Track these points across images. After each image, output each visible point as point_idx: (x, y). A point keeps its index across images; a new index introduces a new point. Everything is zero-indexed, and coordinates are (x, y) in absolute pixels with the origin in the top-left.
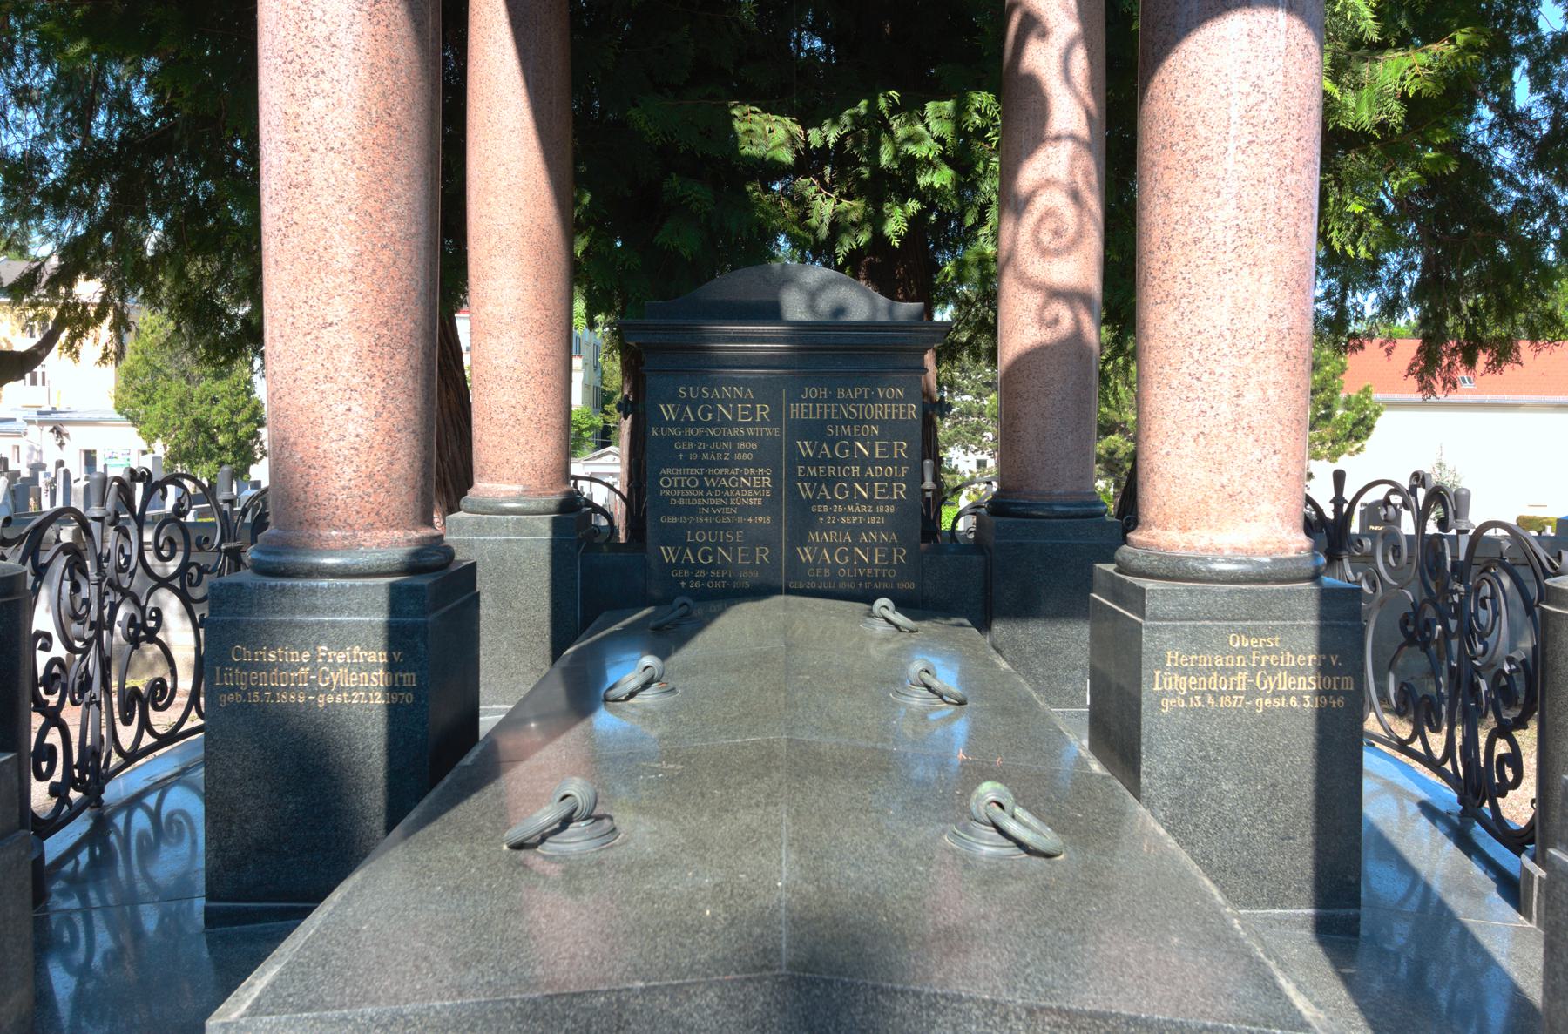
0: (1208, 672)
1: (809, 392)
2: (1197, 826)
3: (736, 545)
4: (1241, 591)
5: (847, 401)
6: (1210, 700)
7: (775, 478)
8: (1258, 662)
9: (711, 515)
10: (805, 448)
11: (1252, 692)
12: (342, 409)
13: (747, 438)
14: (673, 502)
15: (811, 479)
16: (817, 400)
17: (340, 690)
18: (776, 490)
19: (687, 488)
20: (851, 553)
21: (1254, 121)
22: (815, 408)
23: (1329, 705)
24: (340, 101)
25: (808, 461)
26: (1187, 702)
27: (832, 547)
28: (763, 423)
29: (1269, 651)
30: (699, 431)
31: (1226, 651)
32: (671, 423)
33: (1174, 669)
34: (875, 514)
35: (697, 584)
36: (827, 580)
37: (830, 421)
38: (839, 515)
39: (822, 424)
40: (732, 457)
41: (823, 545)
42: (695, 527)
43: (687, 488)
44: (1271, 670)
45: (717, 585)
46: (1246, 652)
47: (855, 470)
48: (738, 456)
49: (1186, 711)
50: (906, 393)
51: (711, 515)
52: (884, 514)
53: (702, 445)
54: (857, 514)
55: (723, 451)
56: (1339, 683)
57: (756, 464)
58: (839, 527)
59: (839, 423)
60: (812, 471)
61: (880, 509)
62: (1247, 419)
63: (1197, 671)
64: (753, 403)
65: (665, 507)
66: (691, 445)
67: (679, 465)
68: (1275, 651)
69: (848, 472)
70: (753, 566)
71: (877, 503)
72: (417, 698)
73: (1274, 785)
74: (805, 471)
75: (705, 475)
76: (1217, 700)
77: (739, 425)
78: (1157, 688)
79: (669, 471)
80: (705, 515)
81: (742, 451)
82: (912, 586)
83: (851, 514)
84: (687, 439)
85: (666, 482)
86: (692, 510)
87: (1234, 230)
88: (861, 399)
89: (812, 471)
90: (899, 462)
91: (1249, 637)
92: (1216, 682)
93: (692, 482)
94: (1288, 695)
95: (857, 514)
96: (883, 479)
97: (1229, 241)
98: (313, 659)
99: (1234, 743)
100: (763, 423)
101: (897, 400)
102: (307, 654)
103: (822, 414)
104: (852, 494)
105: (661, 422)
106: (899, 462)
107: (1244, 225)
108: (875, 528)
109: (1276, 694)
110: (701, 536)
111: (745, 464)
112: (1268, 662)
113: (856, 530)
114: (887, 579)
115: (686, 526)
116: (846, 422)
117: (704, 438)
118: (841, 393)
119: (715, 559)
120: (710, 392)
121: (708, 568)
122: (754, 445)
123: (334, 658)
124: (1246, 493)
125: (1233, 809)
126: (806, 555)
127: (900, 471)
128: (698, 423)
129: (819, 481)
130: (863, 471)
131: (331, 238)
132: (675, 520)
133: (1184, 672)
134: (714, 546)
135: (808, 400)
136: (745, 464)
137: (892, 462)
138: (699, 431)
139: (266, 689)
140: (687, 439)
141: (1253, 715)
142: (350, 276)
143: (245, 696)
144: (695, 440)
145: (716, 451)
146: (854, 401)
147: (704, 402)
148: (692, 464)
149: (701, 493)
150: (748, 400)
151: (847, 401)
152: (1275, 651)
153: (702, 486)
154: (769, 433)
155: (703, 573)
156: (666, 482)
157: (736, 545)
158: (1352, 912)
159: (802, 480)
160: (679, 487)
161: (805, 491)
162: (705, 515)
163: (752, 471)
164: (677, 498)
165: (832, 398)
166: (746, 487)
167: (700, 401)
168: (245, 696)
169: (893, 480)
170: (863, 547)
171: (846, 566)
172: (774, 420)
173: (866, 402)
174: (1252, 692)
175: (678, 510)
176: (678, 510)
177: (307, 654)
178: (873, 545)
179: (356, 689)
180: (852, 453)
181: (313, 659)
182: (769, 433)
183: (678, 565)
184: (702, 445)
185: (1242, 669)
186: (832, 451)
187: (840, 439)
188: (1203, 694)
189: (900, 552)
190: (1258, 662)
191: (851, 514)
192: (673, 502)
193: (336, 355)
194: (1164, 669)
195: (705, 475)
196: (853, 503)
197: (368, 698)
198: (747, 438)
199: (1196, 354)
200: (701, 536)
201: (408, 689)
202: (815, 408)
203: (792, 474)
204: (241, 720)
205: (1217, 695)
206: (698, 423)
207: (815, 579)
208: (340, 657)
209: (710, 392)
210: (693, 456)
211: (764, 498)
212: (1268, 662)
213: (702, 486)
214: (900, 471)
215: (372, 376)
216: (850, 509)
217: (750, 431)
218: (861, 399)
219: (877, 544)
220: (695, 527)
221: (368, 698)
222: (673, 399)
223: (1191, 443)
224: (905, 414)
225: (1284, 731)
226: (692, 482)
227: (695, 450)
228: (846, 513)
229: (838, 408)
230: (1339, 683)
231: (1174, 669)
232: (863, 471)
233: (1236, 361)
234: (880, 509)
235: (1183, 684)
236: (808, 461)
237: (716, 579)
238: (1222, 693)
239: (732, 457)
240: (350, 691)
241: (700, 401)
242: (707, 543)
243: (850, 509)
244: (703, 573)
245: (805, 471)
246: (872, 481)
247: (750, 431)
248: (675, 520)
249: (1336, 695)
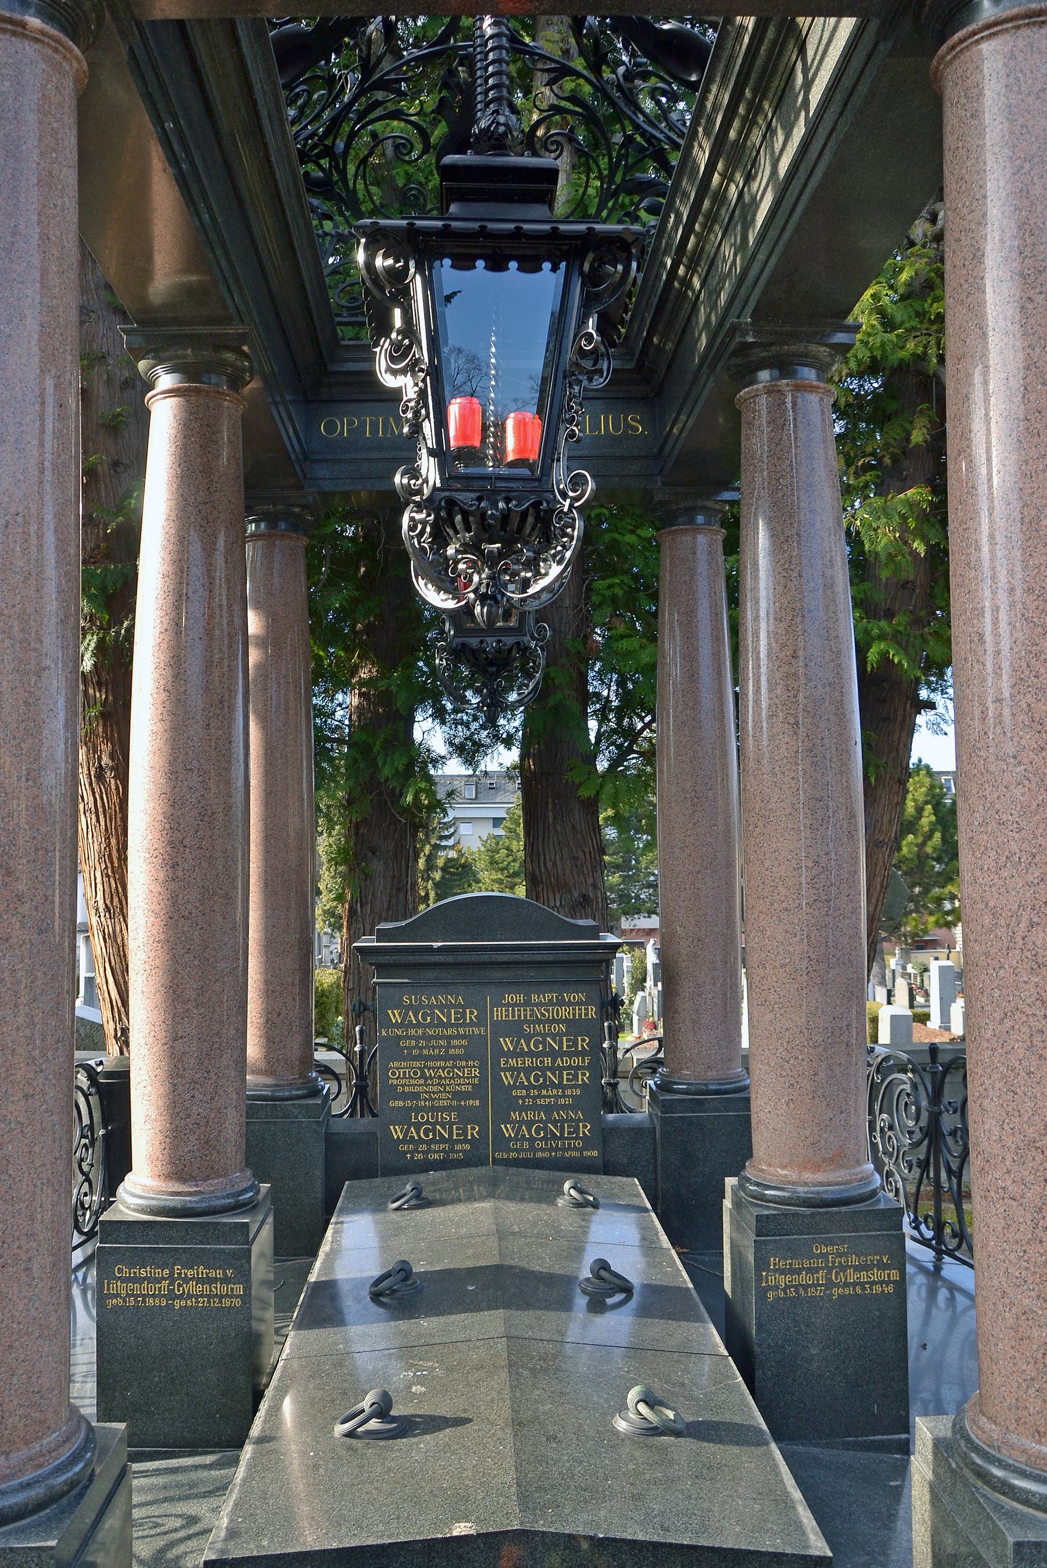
0: (798, 1271)
1: (508, 998)
2: (794, 1380)
3: (451, 1124)
4: (820, 1213)
5: (539, 1005)
6: (801, 1291)
7: (483, 1068)
8: (834, 1262)
9: (431, 1099)
10: (506, 1044)
11: (830, 1285)
12: (188, 1096)
13: (459, 1037)
14: (400, 1089)
15: (512, 1069)
16: (515, 1005)
17: (190, 1296)
18: (483, 1078)
19: (411, 1077)
20: (545, 1129)
21: (817, 886)
22: (513, 1010)
23: (883, 1291)
24: (189, 884)
25: (509, 1054)
26: (785, 1293)
27: (529, 1124)
28: (472, 1024)
29: (840, 1255)
30: (420, 1032)
31: (811, 1256)
32: (397, 1025)
33: (775, 1271)
34: (564, 1096)
35: (420, 1156)
36: (526, 1150)
37: (526, 1021)
38: (534, 1098)
39: (520, 1023)
40: (447, 1051)
41: (522, 1122)
42: (418, 1110)
43: (411, 1077)
44: (843, 1268)
45: (436, 1156)
46: (824, 1256)
47: (547, 1061)
48: (452, 1052)
49: (784, 1299)
50: (586, 997)
51: (431, 1099)
52: (572, 1096)
53: (422, 1043)
54: (549, 1097)
55: (440, 1047)
56: (889, 1275)
57: (466, 1058)
58: (535, 1108)
59: (534, 1023)
60: (512, 1062)
61: (568, 1092)
62: (822, 1090)
63: (792, 1271)
64: (464, 1008)
65: (392, 1092)
66: (413, 1042)
67: (404, 1059)
68: (844, 1254)
69: (542, 1062)
70: (466, 1141)
71: (565, 1088)
72: (244, 1302)
73: (847, 1349)
74: (507, 1062)
75: (426, 1067)
76: (806, 1292)
77: (452, 1026)
78: (764, 1284)
79: (396, 1064)
80: (426, 1100)
81: (455, 1047)
82: (595, 1153)
83: (544, 1097)
84: (411, 1038)
85: (394, 1073)
86: (415, 1096)
87: (807, 960)
88: (551, 1003)
89: (512, 1062)
90: (583, 1053)
91: (826, 1246)
92: (804, 1278)
93: (415, 1073)
94: (854, 1285)
95: (549, 1097)
96: (570, 1067)
97: (804, 967)
98: (172, 1274)
99: (818, 1321)
100: (472, 1024)
101: (580, 1003)
102: (166, 1271)
103: (520, 1016)
104: (545, 1080)
105: (389, 1024)
106: (583, 1053)
107: (813, 956)
108: (564, 1107)
109: (846, 1285)
110: (423, 1117)
111: (459, 1057)
112: (840, 1262)
113: (548, 1109)
114: (575, 1149)
115: (410, 1109)
116: (539, 1022)
117: (424, 1037)
118: (534, 998)
119: (434, 1135)
120: (429, 999)
121: (429, 1143)
122: (464, 1042)
123: (186, 1274)
124: (823, 1142)
125: (819, 1368)
126: (508, 1130)
127: (583, 1061)
128: (419, 1025)
129: (518, 1070)
130: (554, 1061)
131: (182, 978)
132: (401, 1104)
133: (783, 1272)
134: (434, 1125)
135: (508, 1005)
136: (459, 1057)
137: (577, 1054)
138: (420, 1032)
139: (138, 1296)
140: (411, 1038)
141: (831, 1300)
142: (194, 1004)
143: (125, 1301)
144: (417, 1038)
145: (434, 1047)
146: (545, 1004)
147: (424, 1007)
148: (415, 1058)
149: (422, 1081)
150: (460, 1006)
151: (539, 1005)
152: (844, 1254)
153: (423, 1076)
154: (476, 1032)
155: (424, 1147)
156: (394, 1073)
157: (451, 1124)
158: (904, 1436)
159: (505, 1070)
160: (405, 1077)
161: (507, 1079)
162: (426, 1100)
163: (464, 1063)
164: (403, 1086)
165: (527, 1003)
166: (459, 1077)
167: (420, 1007)
168: (125, 1301)
169: (578, 1068)
170: (555, 1123)
171: (541, 1139)
172: (481, 1022)
173: (554, 1005)
174: (830, 1285)
175: (404, 1096)
176: (404, 1096)
177: (166, 1271)
178: (563, 1121)
179: (201, 1296)
180: (544, 1047)
181: (172, 1274)
182: (476, 1032)
183: (404, 1141)
184: (422, 1043)
185: (822, 1268)
186: (528, 1045)
187: (534, 1035)
188: (796, 1287)
189: (585, 1127)
190: (834, 1262)
191: (544, 1097)
192: (400, 1089)
193: (185, 1059)
194: (768, 1270)
195: (426, 1067)
196: (546, 1088)
197: (209, 1302)
198: (459, 1037)
199: (785, 1044)
200: (423, 1117)
201: (237, 1296)
202: (513, 1010)
203: (496, 1064)
204: (121, 1318)
205: (806, 1287)
206: (419, 1025)
207: (516, 1150)
208: (190, 1273)
209: (429, 999)
210: (415, 1052)
211: (474, 1085)
212: (840, 1262)
213: (423, 1076)
214: (583, 1061)
215: (208, 1072)
216: (544, 1092)
217: (461, 1031)
218: (551, 1003)
219: (565, 1068)
220: (418, 1110)
221: (209, 1302)
222: (399, 1005)
223: (785, 1106)
224: (586, 1014)
225: (852, 1311)
226: (415, 1073)
227: (416, 1047)
228: (540, 1096)
229: (532, 1010)
230: (889, 1275)
231: (775, 1271)
232: (554, 1061)
233: (811, 1050)
234: (568, 1092)
235: (783, 1280)
236: (509, 1054)
237: (435, 1152)
238: (809, 1286)
239: (447, 1051)
240: (197, 1297)
241: (420, 1007)
242: (427, 1122)
243: (544, 1092)
244: (424, 1147)
245: (507, 1062)
246: (561, 1069)
247: (461, 1031)
248: (401, 1104)
249: (888, 1283)
